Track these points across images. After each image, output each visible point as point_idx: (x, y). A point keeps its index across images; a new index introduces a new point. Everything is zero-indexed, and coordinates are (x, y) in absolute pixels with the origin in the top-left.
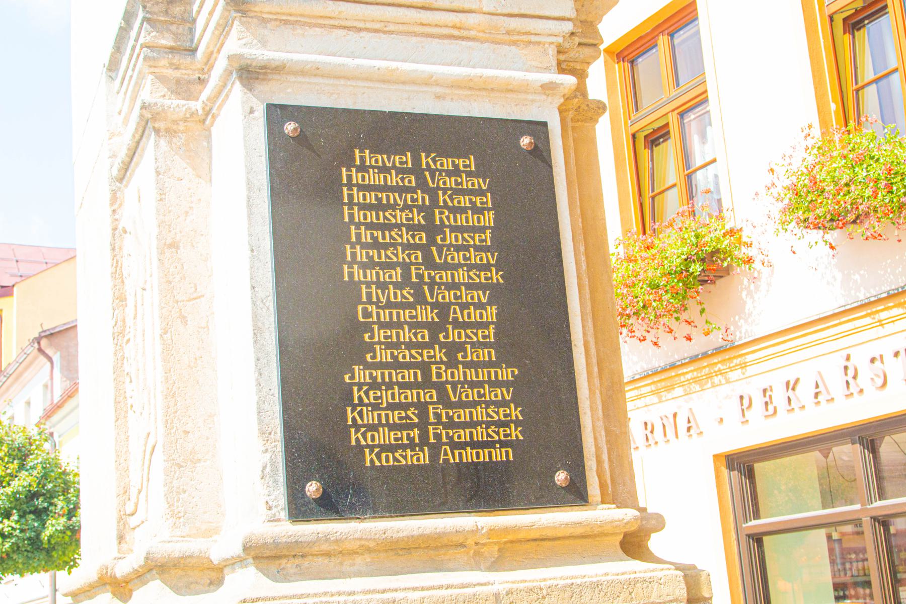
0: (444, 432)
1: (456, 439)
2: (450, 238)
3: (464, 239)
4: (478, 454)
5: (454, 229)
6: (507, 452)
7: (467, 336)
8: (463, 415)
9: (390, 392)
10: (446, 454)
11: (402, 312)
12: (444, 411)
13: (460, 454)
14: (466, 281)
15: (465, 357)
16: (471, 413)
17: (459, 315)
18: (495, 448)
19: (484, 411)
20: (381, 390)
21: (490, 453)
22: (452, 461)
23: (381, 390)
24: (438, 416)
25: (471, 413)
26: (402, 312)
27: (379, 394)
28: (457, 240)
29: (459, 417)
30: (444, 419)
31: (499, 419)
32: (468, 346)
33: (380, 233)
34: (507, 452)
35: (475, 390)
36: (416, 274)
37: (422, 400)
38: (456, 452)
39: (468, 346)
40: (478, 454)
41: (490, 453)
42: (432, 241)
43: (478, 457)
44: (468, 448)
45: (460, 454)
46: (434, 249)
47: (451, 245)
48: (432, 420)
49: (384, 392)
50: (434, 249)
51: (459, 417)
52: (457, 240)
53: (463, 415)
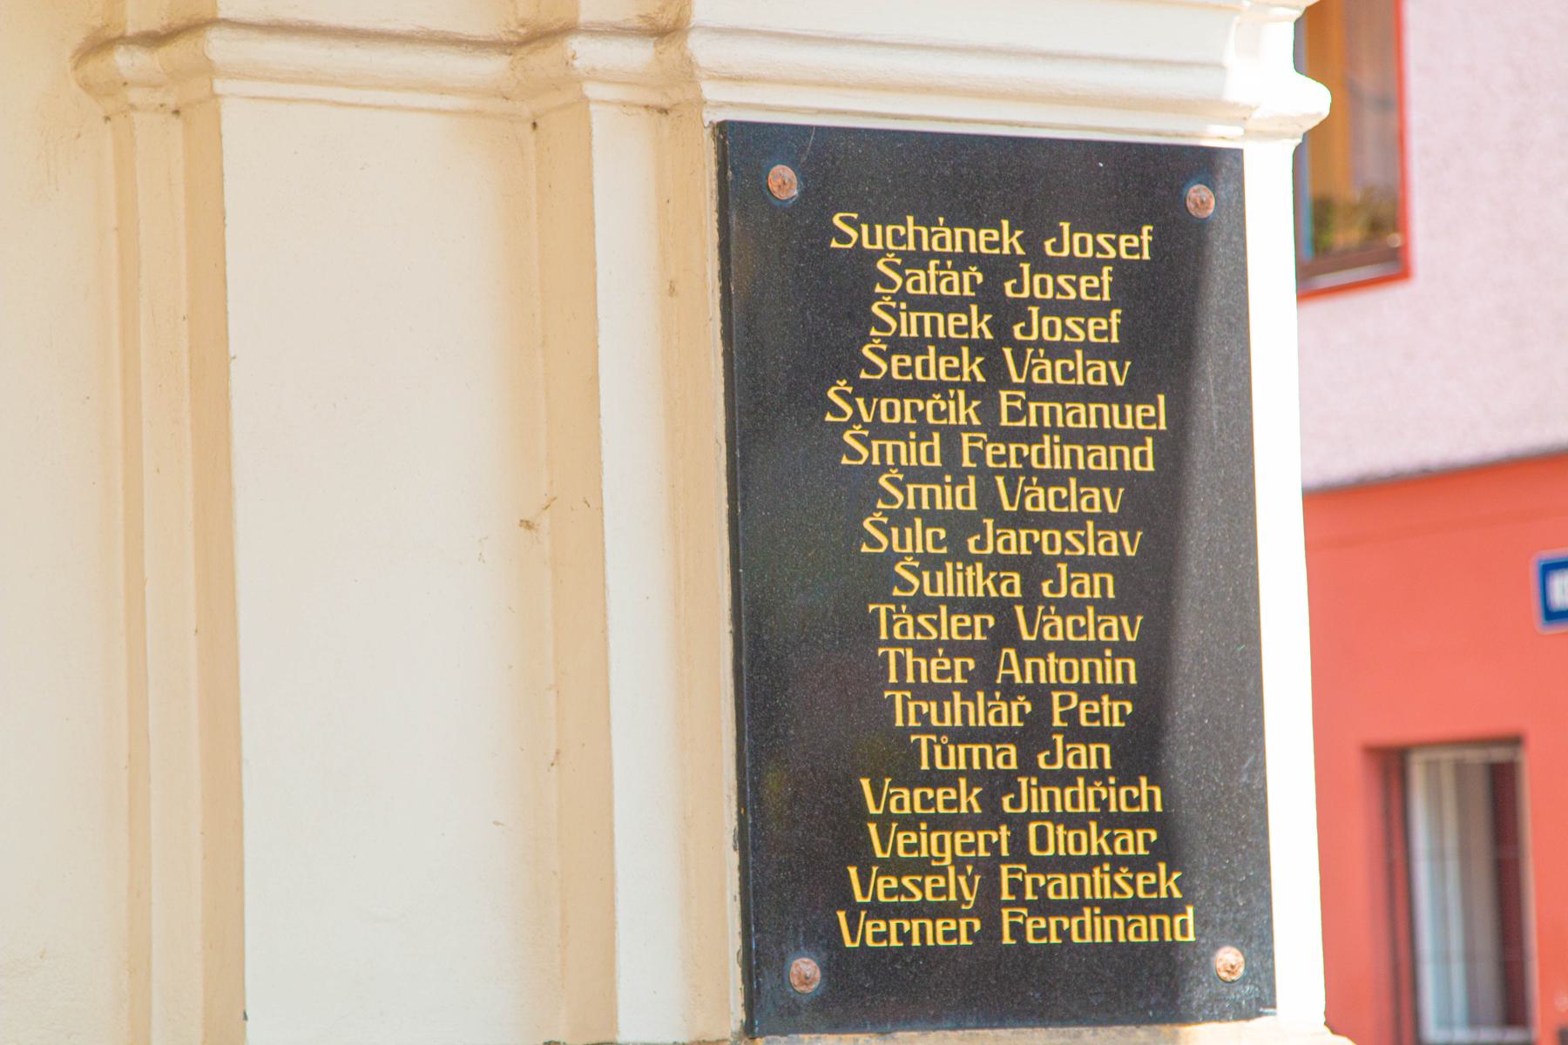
0: (1029, 879)
1: (1051, 895)
2: (1040, 326)
3: (1066, 330)
4: (1069, 667)
5: (1048, 308)
6: (1125, 667)
7: (1066, 544)
8: (1064, 886)
9: (924, 446)
10: (1008, 666)
11: (940, 318)
12: (1029, 879)
13: (1035, 667)
14: (1108, 896)
15: (1055, 588)
16: (1081, 882)
17: (1016, 671)
18: (1103, 658)
19: (1107, 878)
20: (918, 830)
21: (1092, 668)
22: (1018, 680)
23: (918, 830)
24: (1017, 887)
25: (1081, 882)
26: (940, 318)
27: (914, 840)
28: (1043, 290)
29: (1058, 890)
30: (1029, 896)
31: (1100, 489)
32: (1063, 567)
33: (934, 705)
34: (1125, 667)
35: (1070, 620)
36: (1012, 925)
37: (990, 766)
38: (1029, 662)
39: (1063, 567)
40: (1069, 667)
41: (1092, 668)
42: (1001, 329)
43: (1078, 847)
44: (1052, 656)
45: (1035, 667)
46: (1007, 352)
47: (1040, 342)
48: (1006, 896)
49: (924, 836)
50: (1007, 352)
51: (1058, 890)
52: (1043, 290)
53: (1064, 886)
